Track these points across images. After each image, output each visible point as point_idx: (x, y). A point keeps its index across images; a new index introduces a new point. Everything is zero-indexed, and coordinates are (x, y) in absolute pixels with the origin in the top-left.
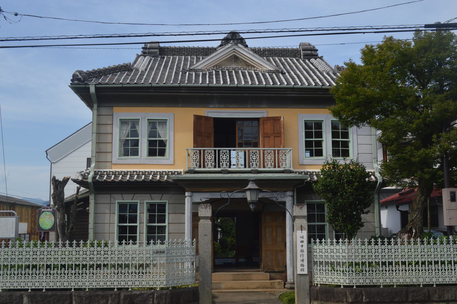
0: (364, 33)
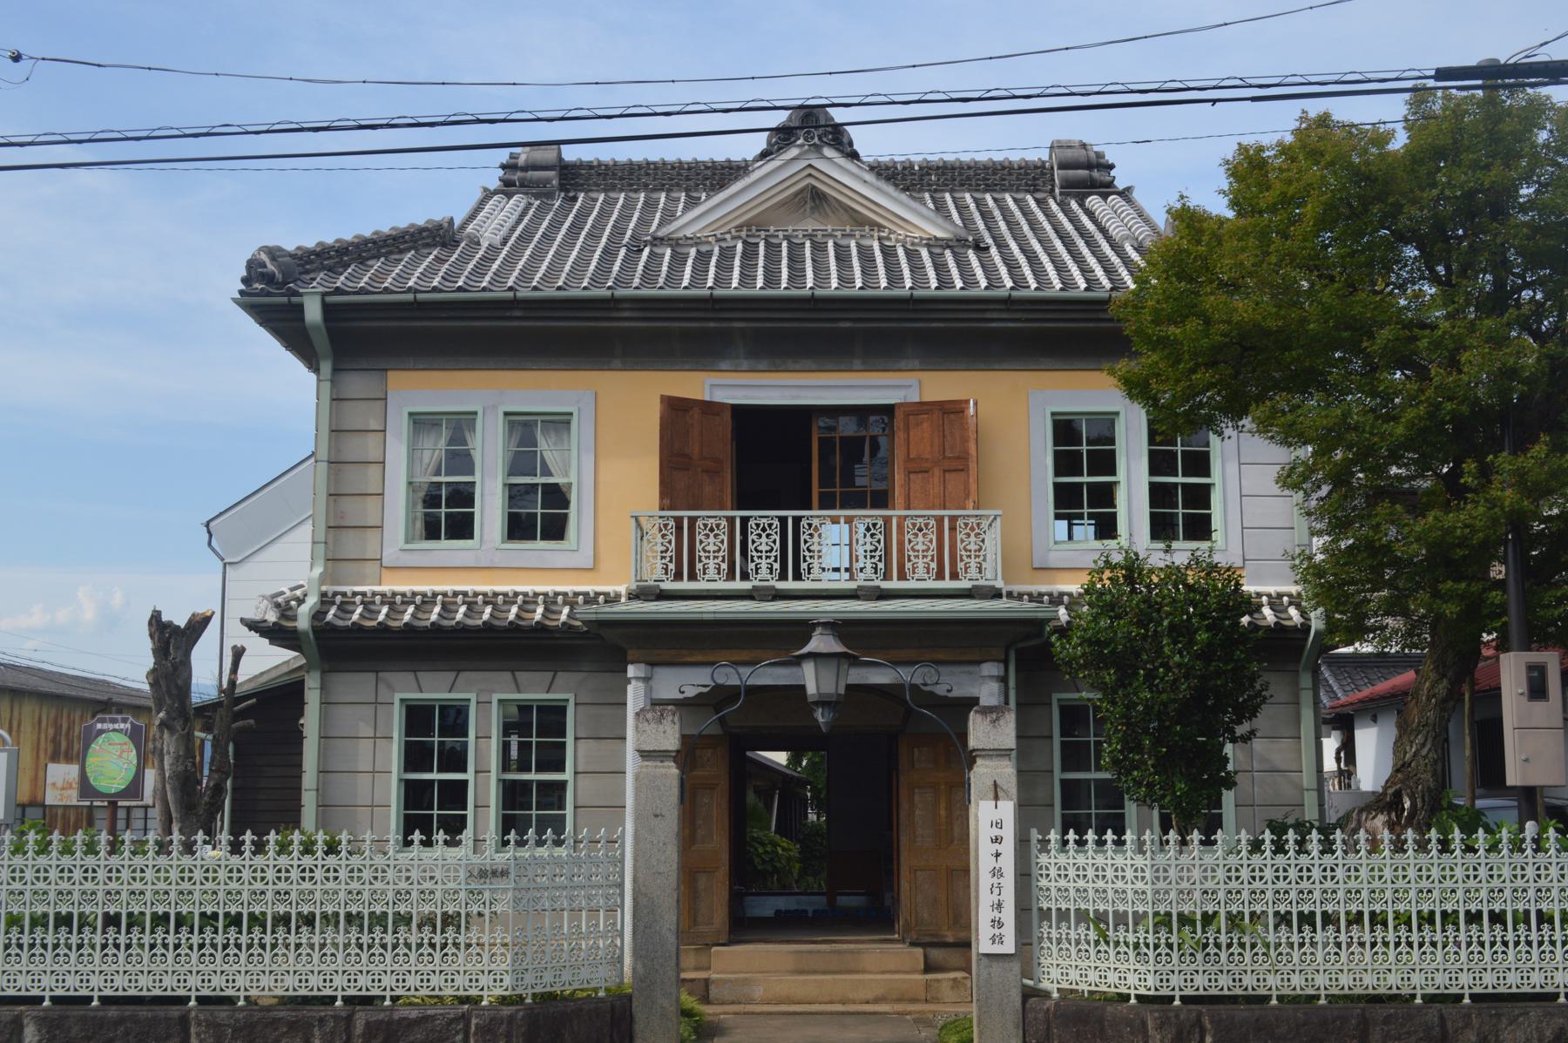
0: (1214, 101)
